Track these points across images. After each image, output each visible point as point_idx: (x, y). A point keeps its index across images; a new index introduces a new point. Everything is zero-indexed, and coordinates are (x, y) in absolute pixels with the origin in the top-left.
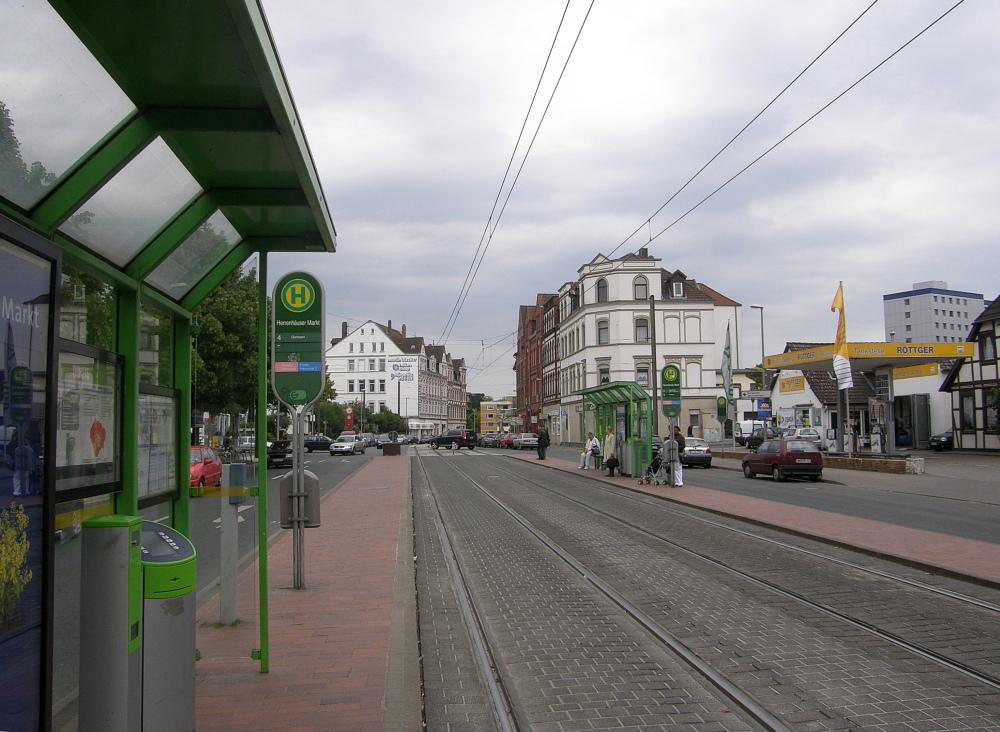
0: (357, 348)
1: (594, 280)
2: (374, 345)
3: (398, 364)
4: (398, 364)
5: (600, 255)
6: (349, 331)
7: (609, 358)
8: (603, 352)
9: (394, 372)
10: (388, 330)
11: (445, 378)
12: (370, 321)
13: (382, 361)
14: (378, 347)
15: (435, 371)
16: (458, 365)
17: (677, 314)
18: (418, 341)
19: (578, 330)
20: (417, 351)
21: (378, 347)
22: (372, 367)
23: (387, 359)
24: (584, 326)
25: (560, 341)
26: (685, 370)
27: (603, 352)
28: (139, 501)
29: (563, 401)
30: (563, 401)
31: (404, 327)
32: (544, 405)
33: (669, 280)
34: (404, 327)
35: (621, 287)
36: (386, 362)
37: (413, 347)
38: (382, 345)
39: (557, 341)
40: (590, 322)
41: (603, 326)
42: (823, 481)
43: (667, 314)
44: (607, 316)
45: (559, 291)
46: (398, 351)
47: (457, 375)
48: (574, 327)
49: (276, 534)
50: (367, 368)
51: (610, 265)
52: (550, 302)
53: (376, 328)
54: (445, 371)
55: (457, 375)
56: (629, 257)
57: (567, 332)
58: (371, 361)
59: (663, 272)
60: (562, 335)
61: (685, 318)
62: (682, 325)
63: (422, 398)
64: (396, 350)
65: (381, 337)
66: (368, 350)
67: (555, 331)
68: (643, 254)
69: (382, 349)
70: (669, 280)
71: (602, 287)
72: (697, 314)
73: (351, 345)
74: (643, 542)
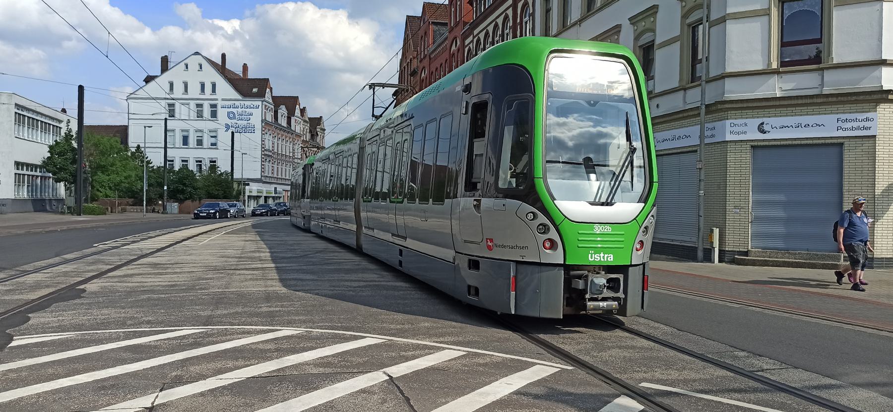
0: (178, 91)
2: (203, 86)
3: (234, 110)
4: (234, 110)
6: (170, 65)
9: (229, 122)
10: (221, 68)
11: (299, 136)
12: (197, 53)
13: (214, 106)
14: (208, 88)
15: (284, 124)
16: (315, 123)
20: (261, 95)
21: (208, 88)
22: (200, 115)
23: (220, 103)
31: (245, 67)
34: (245, 67)
36: (219, 107)
37: (255, 90)
38: (214, 86)
42: (389, 376)
46: (234, 94)
47: (314, 135)
49: (781, 260)
50: (193, 115)
53: (206, 65)
54: (298, 126)
55: (314, 135)
58: (170, 105)
63: (267, 156)
64: (232, 93)
65: (211, 75)
66: (194, 91)
69: (214, 90)
73: (171, 85)
74: (277, 350)
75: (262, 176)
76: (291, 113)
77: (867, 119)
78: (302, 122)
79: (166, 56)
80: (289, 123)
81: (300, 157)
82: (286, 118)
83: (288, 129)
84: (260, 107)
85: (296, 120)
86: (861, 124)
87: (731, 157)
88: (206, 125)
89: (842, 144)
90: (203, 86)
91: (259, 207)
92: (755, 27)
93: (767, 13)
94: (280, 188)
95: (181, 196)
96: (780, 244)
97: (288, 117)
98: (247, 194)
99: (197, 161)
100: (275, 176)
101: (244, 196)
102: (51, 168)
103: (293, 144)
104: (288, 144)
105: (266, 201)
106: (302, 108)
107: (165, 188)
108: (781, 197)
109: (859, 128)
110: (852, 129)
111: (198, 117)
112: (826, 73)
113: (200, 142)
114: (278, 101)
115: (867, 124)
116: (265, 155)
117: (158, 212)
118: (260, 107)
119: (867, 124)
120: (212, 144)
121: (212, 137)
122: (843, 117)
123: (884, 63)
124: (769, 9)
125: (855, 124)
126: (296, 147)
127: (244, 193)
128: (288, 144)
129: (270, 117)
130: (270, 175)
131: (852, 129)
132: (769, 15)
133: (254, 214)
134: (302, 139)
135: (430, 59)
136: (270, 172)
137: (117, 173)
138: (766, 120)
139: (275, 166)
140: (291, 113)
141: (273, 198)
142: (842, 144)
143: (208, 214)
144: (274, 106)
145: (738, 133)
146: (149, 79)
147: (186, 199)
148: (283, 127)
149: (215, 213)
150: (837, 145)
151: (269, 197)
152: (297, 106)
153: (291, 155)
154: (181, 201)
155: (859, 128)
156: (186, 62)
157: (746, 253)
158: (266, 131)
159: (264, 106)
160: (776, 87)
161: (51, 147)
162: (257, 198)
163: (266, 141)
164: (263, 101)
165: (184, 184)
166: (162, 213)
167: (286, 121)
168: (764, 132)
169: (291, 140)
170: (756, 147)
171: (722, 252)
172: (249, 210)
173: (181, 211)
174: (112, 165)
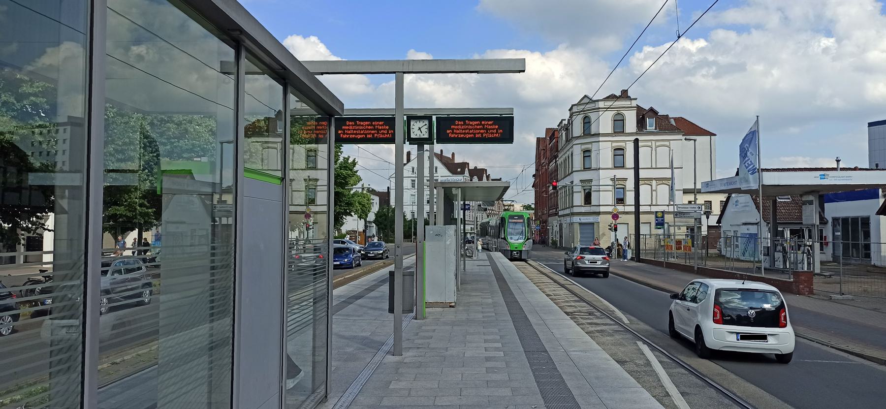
1: (581, 116)
5: (585, 96)
7: (591, 180)
8: (586, 175)
17: (649, 144)
18: (464, 165)
19: (569, 157)
24: (572, 154)
25: (559, 165)
26: (656, 190)
27: (586, 175)
28: (716, 290)
29: (561, 213)
30: (561, 213)
32: (550, 216)
33: (642, 116)
34: (453, 154)
35: (604, 122)
37: (459, 170)
39: (557, 166)
40: (577, 151)
41: (587, 153)
43: (658, 144)
44: (623, 144)
45: (558, 126)
48: (566, 155)
51: (593, 105)
52: (552, 134)
56: (612, 97)
57: (562, 159)
58: (412, 180)
59: (639, 108)
60: (560, 161)
61: (657, 147)
62: (654, 152)
67: (556, 158)
68: (625, 95)
70: (642, 116)
71: (587, 122)
72: (667, 143)
141: (470, 233)
150: (593, 224)
152: (485, 175)
160: (583, 210)
170: (581, 224)
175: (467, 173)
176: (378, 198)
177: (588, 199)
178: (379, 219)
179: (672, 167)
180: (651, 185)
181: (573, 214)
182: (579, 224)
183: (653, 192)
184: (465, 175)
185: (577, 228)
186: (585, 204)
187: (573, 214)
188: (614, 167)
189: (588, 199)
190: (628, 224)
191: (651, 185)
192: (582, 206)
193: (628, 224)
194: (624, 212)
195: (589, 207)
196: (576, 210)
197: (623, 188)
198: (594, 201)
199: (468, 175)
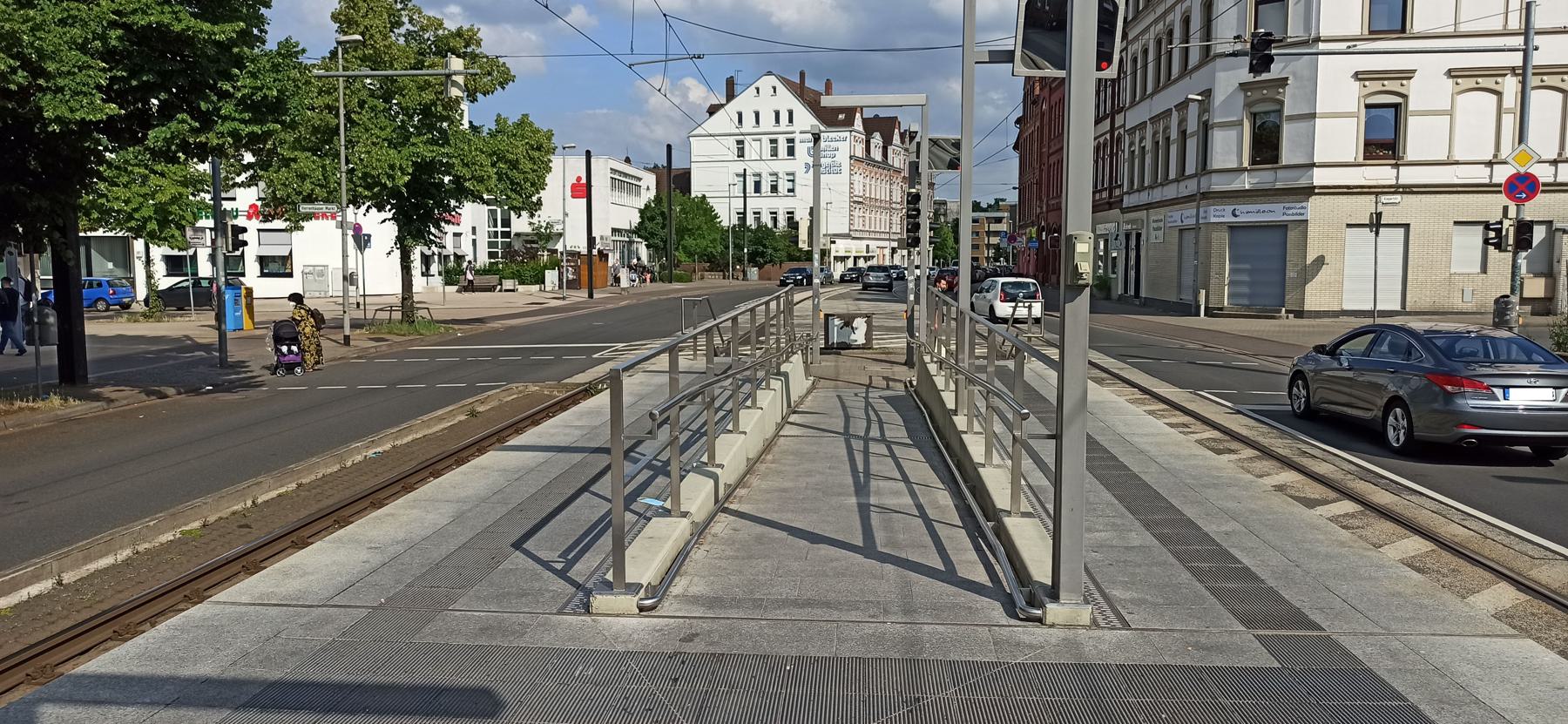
2: (777, 114)
6: (738, 89)
11: (898, 171)
13: (791, 141)
14: (784, 117)
21: (784, 117)
22: (774, 153)
23: (798, 137)
29: (1128, 201)
30: (1128, 201)
38: (791, 113)
48: (1152, 34)
50: (767, 153)
66: (767, 123)
69: (791, 120)
73: (740, 115)
75: (850, 230)
76: (887, 142)
77: (1302, 208)
78: (903, 152)
79: (732, 77)
80: (885, 155)
81: (899, 200)
82: (881, 149)
83: (884, 164)
84: (848, 139)
85: (894, 150)
86: (1299, 211)
87: (1214, 235)
88: (782, 166)
89: (1286, 225)
90: (777, 114)
91: (848, 271)
92: (1232, 134)
93: (1241, 123)
94: (873, 244)
95: (761, 260)
96: (1246, 302)
97: (883, 147)
98: (833, 254)
99: (771, 213)
100: (867, 228)
101: (829, 257)
102: (643, 233)
103: (891, 184)
104: (883, 184)
105: (855, 264)
106: (902, 131)
107: (746, 250)
108: (1247, 266)
109: (1296, 214)
110: (1293, 215)
111: (772, 156)
112: (1278, 171)
113: (774, 188)
114: (871, 126)
115: (1302, 211)
116: (855, 202)
117: (738, 279)
118: (848, 139)
119: (1302, 211)
120: (789, 191)
121: (789, 181)
122: (1287, 205)
123: (1313, 165)
124: (1242, 120)
125: (1294, 211)
126: (894, 187)
127: (829, 253)
128: (883, 184)
129: (860, 151)
130: (861, 228)
131: (1293, 215)
132: (1242, 125)
133: (842, 280)
134: (902, 175)
135: (1051, 89)
136: (861, 225)
137: (704, 237)
138: (1236, 207)
139: (867, 215)
140: (887, 142)
141: (865, 258)
142: (1286, 225)
143: (795, 280)
144: (866, 136)
145: (1219, 216)
146: (713, 110)
147: (766, 263)
148: (879, 162)
149: (802, 280)
150: (1283, 227)
151: (859, 257)
152: (896, 131)
153: (888, 199)
154: (760, 267)
155: (1296, 214)
156: (756, 85)
157: (1221, 309)
158: (856, 170)
159: (852, 137)
160: (1246, 182)
161: (641, 211)
162: (843, 259)
163: (856, 183)
164: (851, 131)
165: (764, 246)
166: (743, 280)
167: (880, 154)
168: (1235, 216)
169: (888, 178)
170: (1233, 228)
171: (1206, 308)
172: (837, 276)
173: (761, 278)
174: (699, 228)
175: (858, 124)
176: (655, 176)
177: (1266, 146)
178: (648, 225)
179: (1527, 32)
180: (1499, 94)
181: (1207, 196)
182: (1230, 227)
183: (1504, 116)
184: (856, 127)
185: (1222, 240)
186: (1253, 162)
187: (1207, 196)
188: (1371, 32)
189: (1266, 146)
190: (1407, 226)
191: (1499, 94)
192: (1245, 170)
193: (1407, 226)
194: (1397, 186)
195: (1272, 172)
196: (1218, 184)
197: (1396, 106)
198: (1289, 153)
199: (861, 129)
